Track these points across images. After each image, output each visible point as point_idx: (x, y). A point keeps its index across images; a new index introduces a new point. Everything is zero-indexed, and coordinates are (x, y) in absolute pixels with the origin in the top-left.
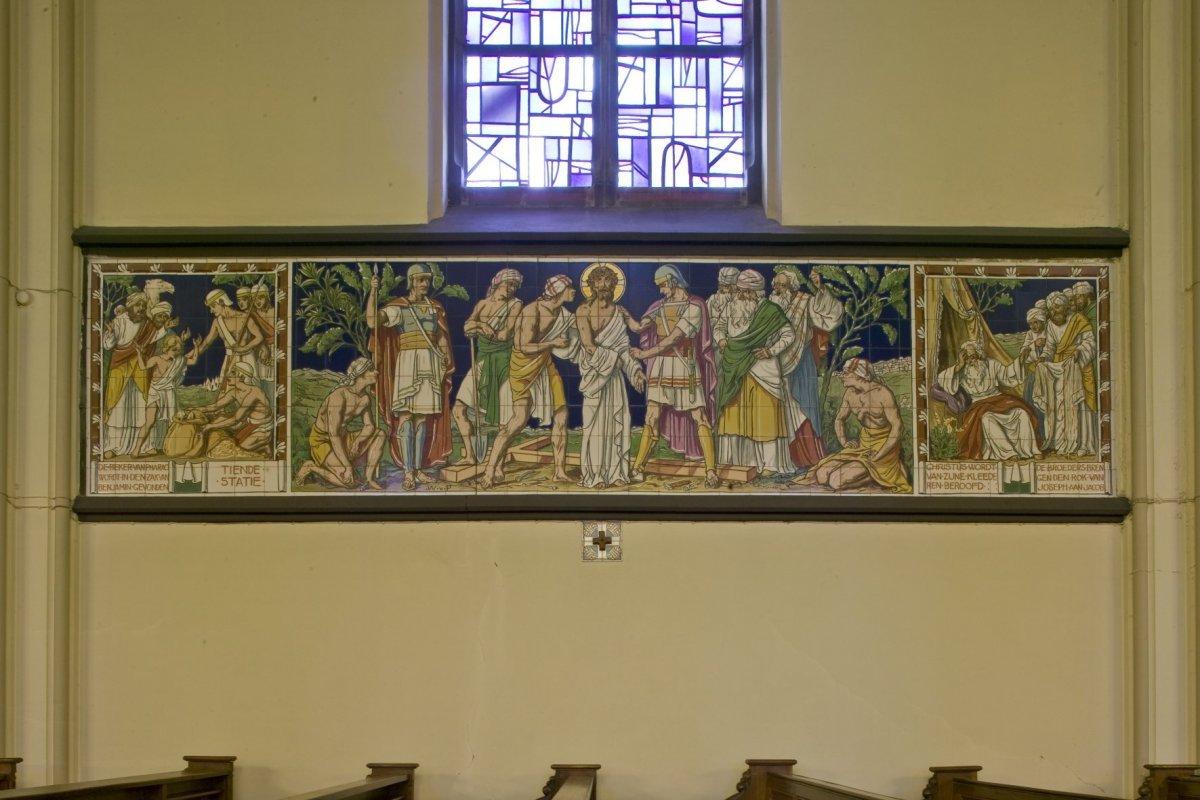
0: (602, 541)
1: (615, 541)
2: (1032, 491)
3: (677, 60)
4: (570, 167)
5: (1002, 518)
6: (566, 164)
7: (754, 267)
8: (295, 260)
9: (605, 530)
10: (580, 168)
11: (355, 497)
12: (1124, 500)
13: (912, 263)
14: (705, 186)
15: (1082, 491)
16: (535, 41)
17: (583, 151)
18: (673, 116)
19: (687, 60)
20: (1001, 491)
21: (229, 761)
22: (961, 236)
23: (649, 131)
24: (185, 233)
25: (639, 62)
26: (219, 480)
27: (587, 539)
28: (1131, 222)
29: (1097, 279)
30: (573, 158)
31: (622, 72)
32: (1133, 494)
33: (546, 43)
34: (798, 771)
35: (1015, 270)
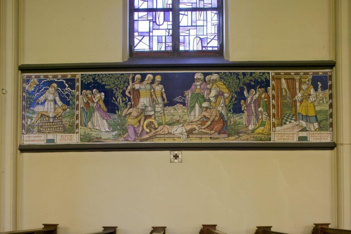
0: (176, 157)
1: (180, 156)
3: (197, 12)
4: (165, 44)
5: (225, 149)
6: (164, 44)
7: (216, 73)
10: (168, 45)
11: (92, 144)
12: (334, 143)
13: (270, 71)
15: (285, 140)
16: (155, 7)
17: (169, 39)
18: (196, 29)
19: (201, 12)
20: (297, 140)
21: (56, 225)
22: (48, 67)
23: (189, 33)
24: (104, 64)
25: (186, 13)
26: (60, 139)
29: (26, 79)
30: (166, 42)
31: (181, 16)
33: (158, 7)
35: (43, 76)
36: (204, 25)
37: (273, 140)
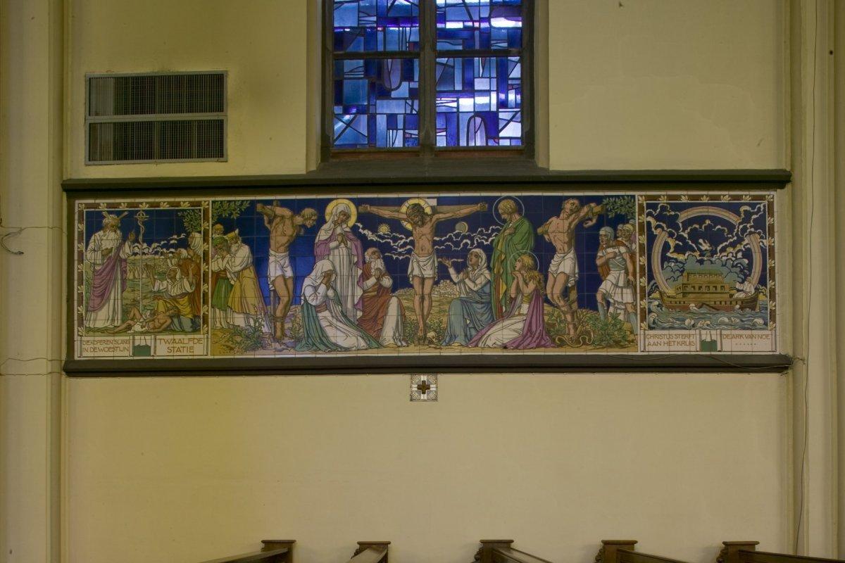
0: (424, 388)
1: (433, 388)
2: (152, 354)
8: (213, 199)
9: (425, 379)
10: (411, 134)
12: (785, 357)
13: (636, 193)
14: (497, 145)
21: (290, 544)
26: (163, 349)
27: (434, 389)
28: (792, 165)
32: (794, 353)
34: (640, 548)
36: (492, 89)
37: (642, 350)
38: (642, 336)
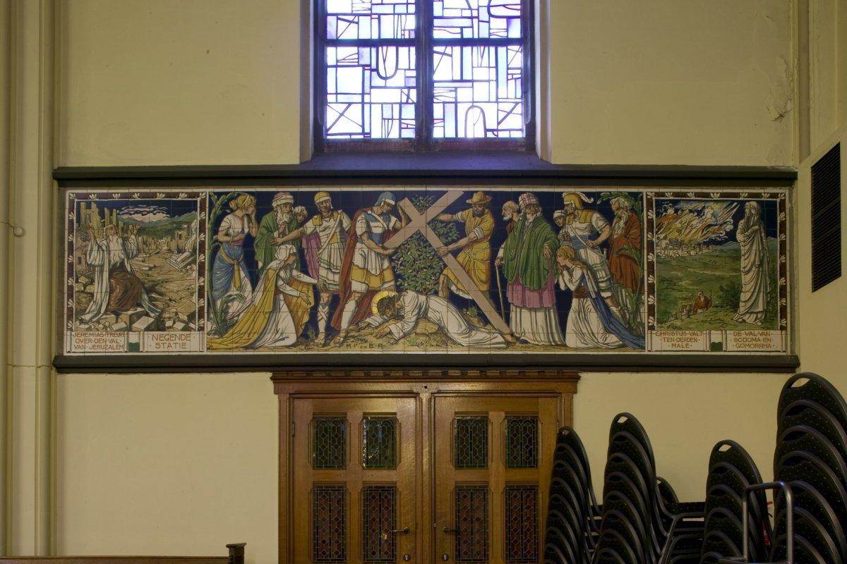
37: (69, 350)
38: (69, 337)
